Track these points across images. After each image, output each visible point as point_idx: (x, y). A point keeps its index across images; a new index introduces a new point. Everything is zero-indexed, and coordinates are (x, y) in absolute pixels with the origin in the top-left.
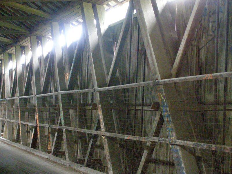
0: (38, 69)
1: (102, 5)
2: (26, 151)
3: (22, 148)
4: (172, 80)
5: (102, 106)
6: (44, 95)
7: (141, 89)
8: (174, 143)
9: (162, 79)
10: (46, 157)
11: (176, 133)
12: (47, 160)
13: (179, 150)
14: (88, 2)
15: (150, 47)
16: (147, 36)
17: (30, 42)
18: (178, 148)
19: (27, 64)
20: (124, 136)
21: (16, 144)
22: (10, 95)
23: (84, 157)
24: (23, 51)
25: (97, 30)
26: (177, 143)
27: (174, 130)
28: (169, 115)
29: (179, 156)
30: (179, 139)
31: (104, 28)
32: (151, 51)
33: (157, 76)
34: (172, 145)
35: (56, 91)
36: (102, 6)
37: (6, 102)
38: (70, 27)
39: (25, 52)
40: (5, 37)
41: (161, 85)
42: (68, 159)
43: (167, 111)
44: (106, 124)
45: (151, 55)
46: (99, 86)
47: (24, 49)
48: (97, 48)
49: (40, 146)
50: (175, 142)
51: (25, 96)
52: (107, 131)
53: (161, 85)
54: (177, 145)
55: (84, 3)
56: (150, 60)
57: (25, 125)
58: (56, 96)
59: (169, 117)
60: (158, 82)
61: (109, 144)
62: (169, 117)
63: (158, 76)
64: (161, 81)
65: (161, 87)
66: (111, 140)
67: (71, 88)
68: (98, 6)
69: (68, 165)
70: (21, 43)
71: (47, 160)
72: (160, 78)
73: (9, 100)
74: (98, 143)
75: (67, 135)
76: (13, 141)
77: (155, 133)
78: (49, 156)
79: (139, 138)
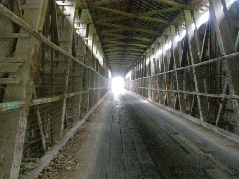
0: (177, 48)
1: (198, 10)
2: (161, 107)
3: (159, 105)
4: (231, 55)
5: (196, 76)
6: (205, 63)
7: (141, 77)
8: (233, 97)
9: (226, 55)
10: (170, 110)
11: (235, 91)
12: (170, 112)
13: (236, 102)
14: (188, 10)
15: (219, 35)
16: (217, 27)
17: (184, 19)
18: (236, 101)
19: (170, 48)
20: (207, 95)
21: (156, 103)
22: (154, 73)
23: (190, 109)
24: (177, 30)
25: (222, 7)
26: (235, 98)
27: (234, 89)
28: (230, 79)
29: (236, 106)
30: (236, 95)
31: (170, 43)
32: (220, 37)
33: (223, 53)
34: (232, 99)
35: (191, 64)
36: (197, 11)
37: (152, 78)
38: (199, 13)
39: (179, 32)
40: (149, 38)
41: (226, 59)
42: (181, 111)
43: (229, 77)
44: (199, 88)
45: (220, 39)
46: (195, 64)
47: (168, 38)
48: (194, 39)
49: (168, 104)
50: (233, 97)
51: (202, 63)
52: (199, 92)
53: (226, 59)
54: (236, 99)
55: (171, 26)
56: (219, 43)
57: (161, 91)
58: (191, 68)
59: (231, 80)
60: (224, 57)
61: (200, 101)
62: (231, 80)
63: (224, 53)
64: (225, 56)
65: (226, 60)
66: (202, 97)
67: (183, 66)
68: (194, 12)
69: (180, 115)
70: (157, 41)
71: (170, 112)
72: (225, 54)
73: (154, 77)
74: (228, 106)
75: (180, 96)
76: (156, 101)
77: (226, 92)
78: (172, 109)
79: (215, 96)
